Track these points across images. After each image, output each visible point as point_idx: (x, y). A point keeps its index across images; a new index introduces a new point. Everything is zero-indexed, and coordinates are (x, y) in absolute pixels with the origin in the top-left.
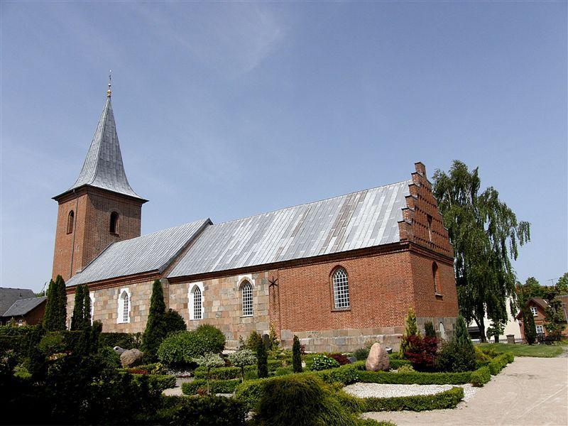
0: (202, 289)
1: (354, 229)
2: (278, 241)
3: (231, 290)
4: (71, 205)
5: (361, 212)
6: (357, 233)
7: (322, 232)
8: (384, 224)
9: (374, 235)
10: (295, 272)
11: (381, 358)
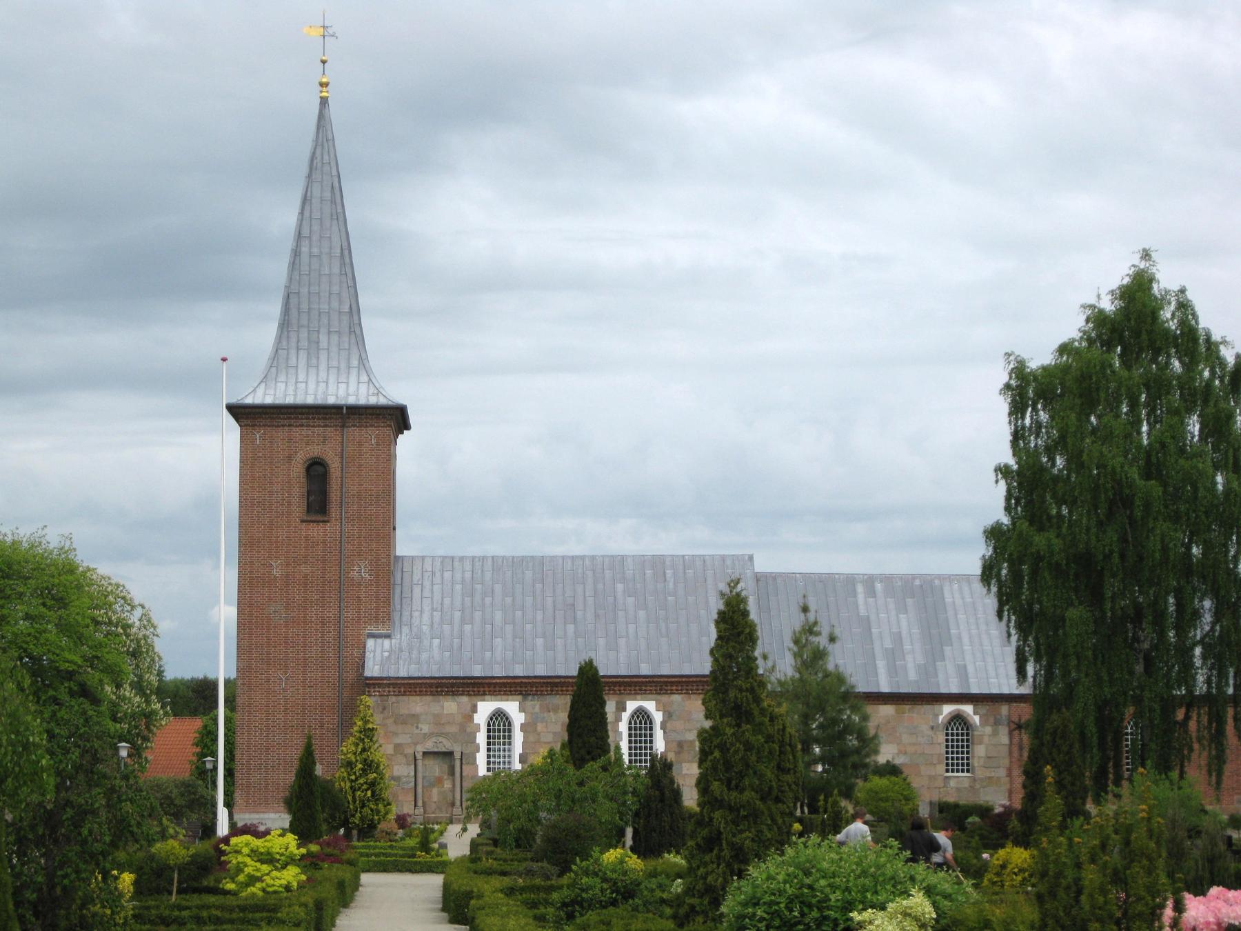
3: (925, 728)
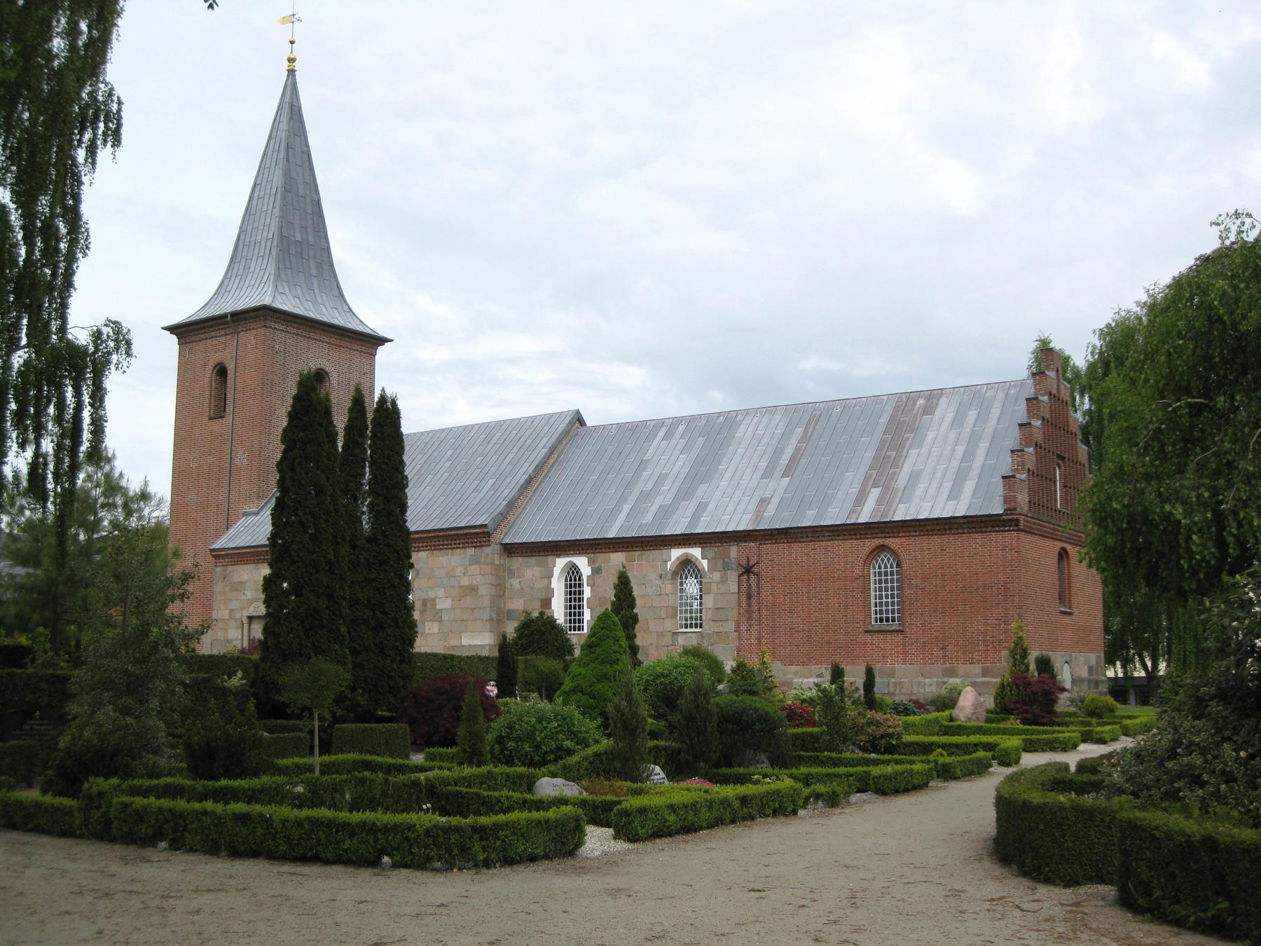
0: (586, 570)
1: (915, 476)
2: (754, 482)
3: (653, 576)
4: (219, 349)
5: (929, 439)
6: (921, 486)
7: (849, 475)
8: (974, 474)
9: (954, 494)
10: (796, 552)
11: (975, 709)
